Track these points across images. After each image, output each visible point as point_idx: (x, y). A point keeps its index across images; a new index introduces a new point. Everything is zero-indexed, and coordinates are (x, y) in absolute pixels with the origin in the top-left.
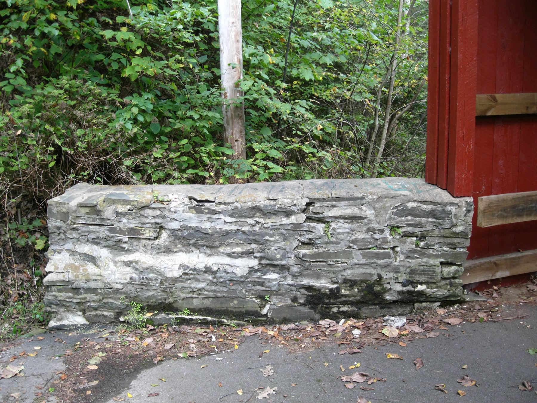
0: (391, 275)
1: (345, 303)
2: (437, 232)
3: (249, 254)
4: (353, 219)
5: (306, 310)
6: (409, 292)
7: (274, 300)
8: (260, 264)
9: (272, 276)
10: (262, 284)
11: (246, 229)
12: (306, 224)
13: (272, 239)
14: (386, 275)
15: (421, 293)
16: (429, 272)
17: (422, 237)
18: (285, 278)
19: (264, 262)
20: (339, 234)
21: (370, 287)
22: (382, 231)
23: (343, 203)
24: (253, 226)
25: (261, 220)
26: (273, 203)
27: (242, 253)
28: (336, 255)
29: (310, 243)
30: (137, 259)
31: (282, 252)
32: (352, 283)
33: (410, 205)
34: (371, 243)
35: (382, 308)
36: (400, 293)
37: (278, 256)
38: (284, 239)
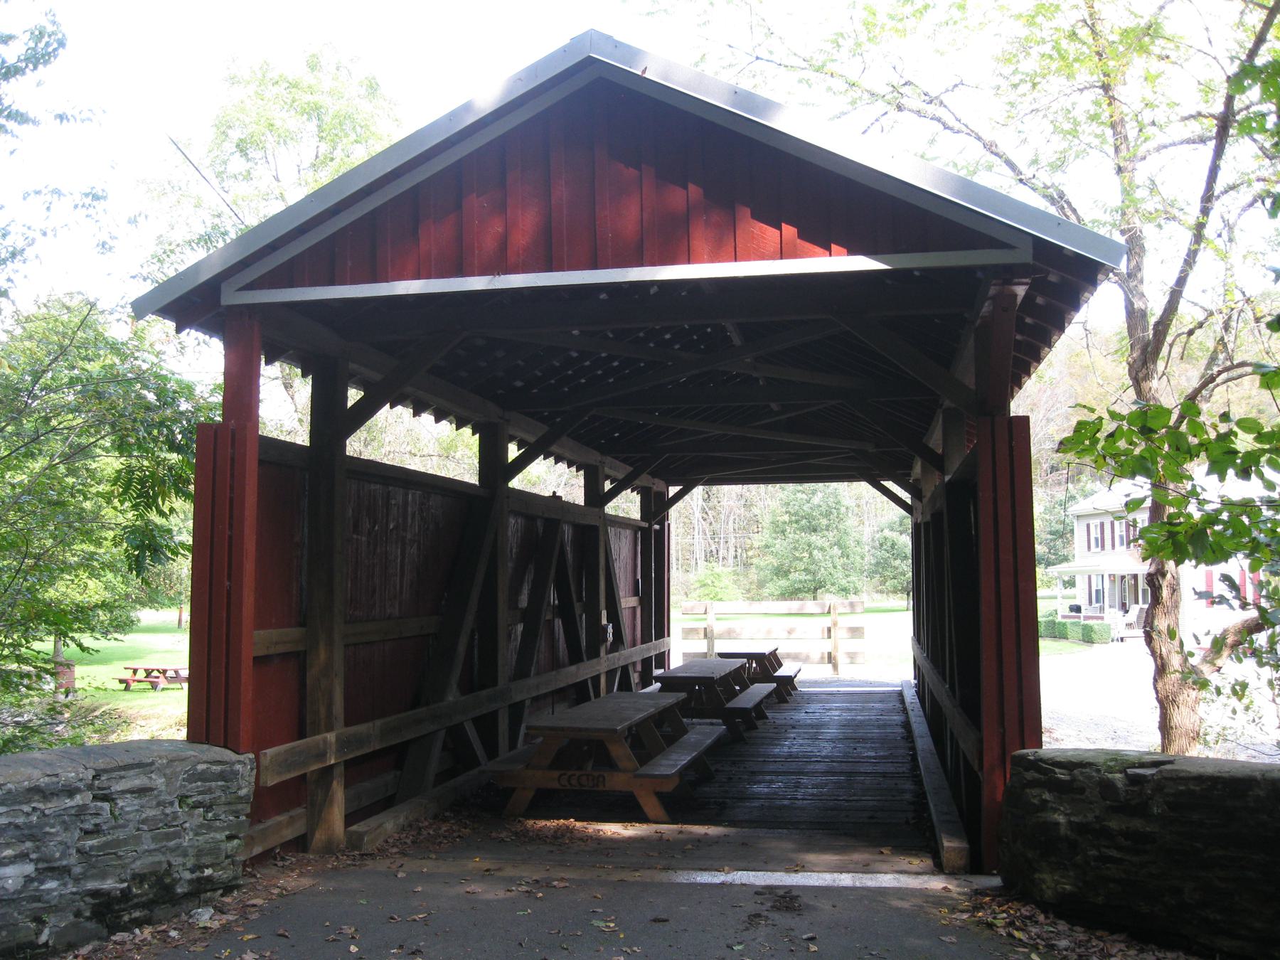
0: (180, 860)
1: (136, 907)
2: (223, 799)
3: (22, 857)
4: (141, 791)
5: (91, 925)
6: (199, 880)
7: (51, 920)
8: (36, 869)
9: (51, 885)
10: (38, 899)
11: (21, 820)
12: (92, 805)
13: (53, 830)
14: (177, 861)
15: (209, 879)
16: (214, 850)
17: (209, 808)
18: (65, 885)
19: (40, 866)
20: (128, 813)
21: (160, 879)
22: (171, 804)
23: (132, 772)
24: (28, 814)
25: (41, 806)
26: (55, 779)
27: (16, 857)
28: (125, 842)
29: (96, 831)
30: (878, 596)
31: (61, 848)
32: (139, 878)
33: (201, 767)
34: (161, 821)
35: (174, 906)
36: (190, 882)
37: (58, 855)
38: (66, 829)
